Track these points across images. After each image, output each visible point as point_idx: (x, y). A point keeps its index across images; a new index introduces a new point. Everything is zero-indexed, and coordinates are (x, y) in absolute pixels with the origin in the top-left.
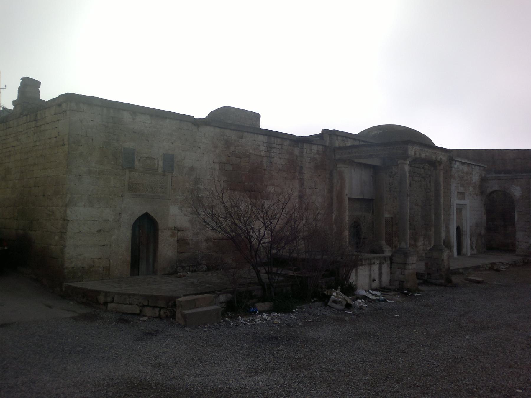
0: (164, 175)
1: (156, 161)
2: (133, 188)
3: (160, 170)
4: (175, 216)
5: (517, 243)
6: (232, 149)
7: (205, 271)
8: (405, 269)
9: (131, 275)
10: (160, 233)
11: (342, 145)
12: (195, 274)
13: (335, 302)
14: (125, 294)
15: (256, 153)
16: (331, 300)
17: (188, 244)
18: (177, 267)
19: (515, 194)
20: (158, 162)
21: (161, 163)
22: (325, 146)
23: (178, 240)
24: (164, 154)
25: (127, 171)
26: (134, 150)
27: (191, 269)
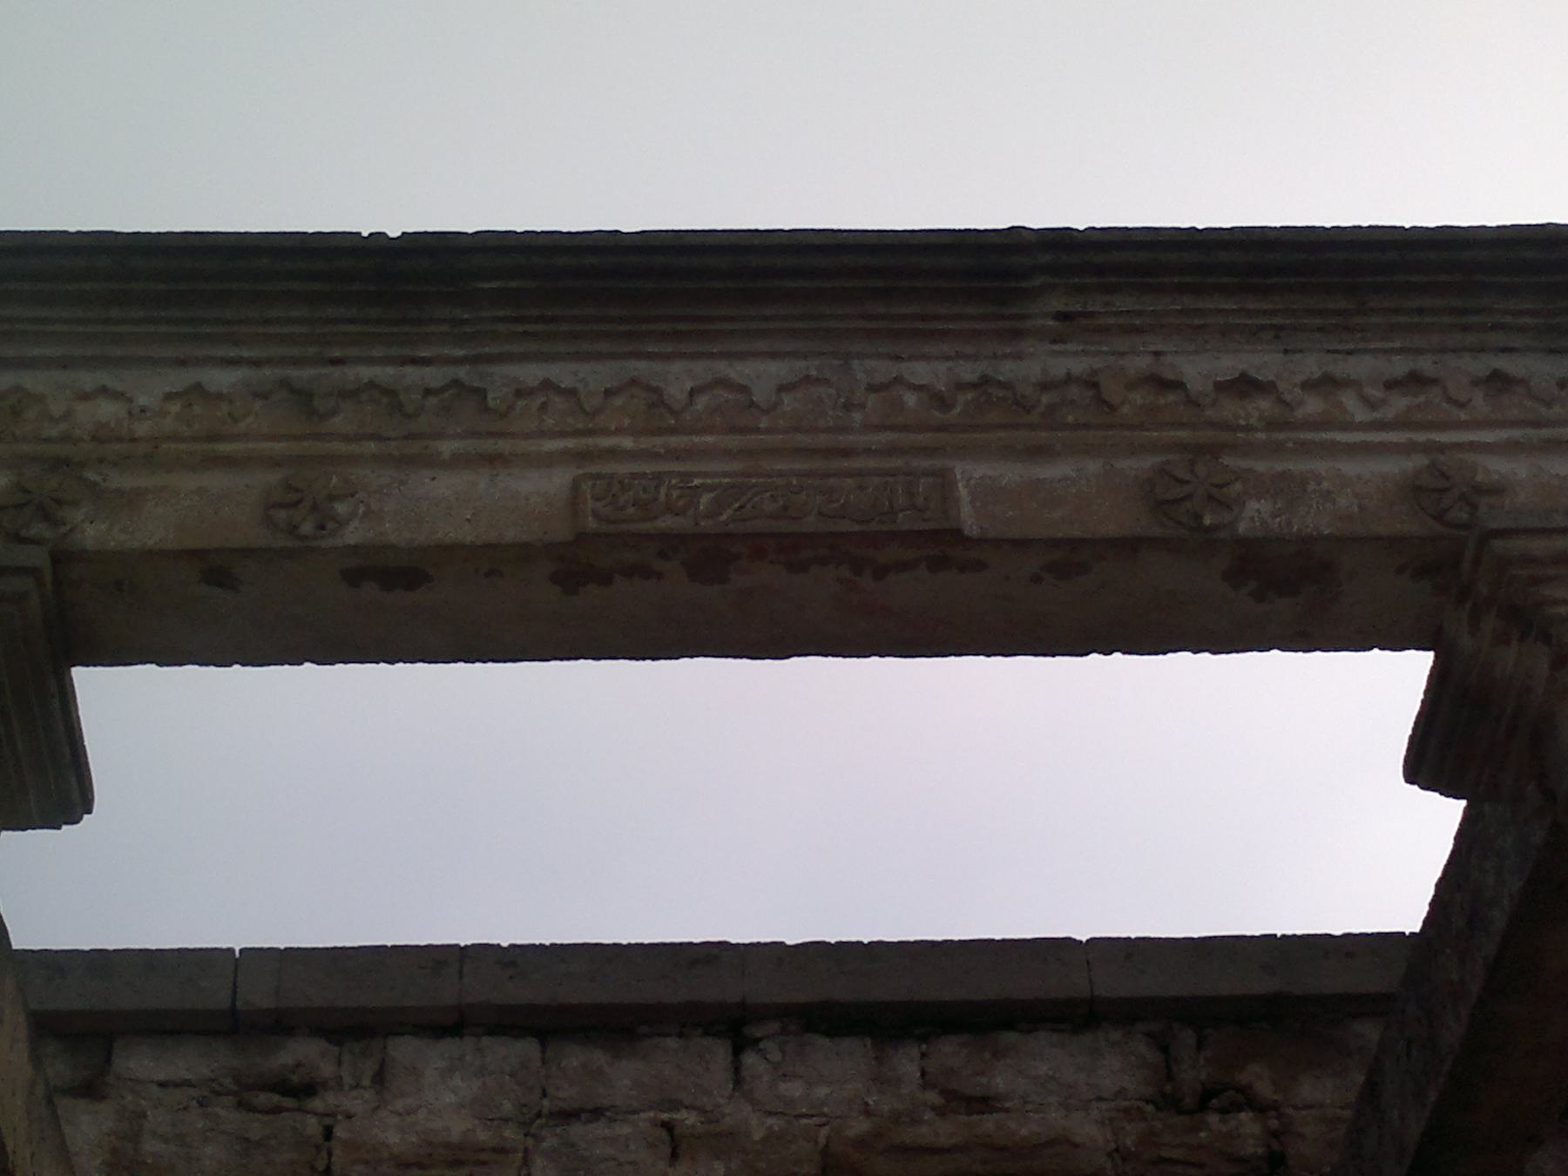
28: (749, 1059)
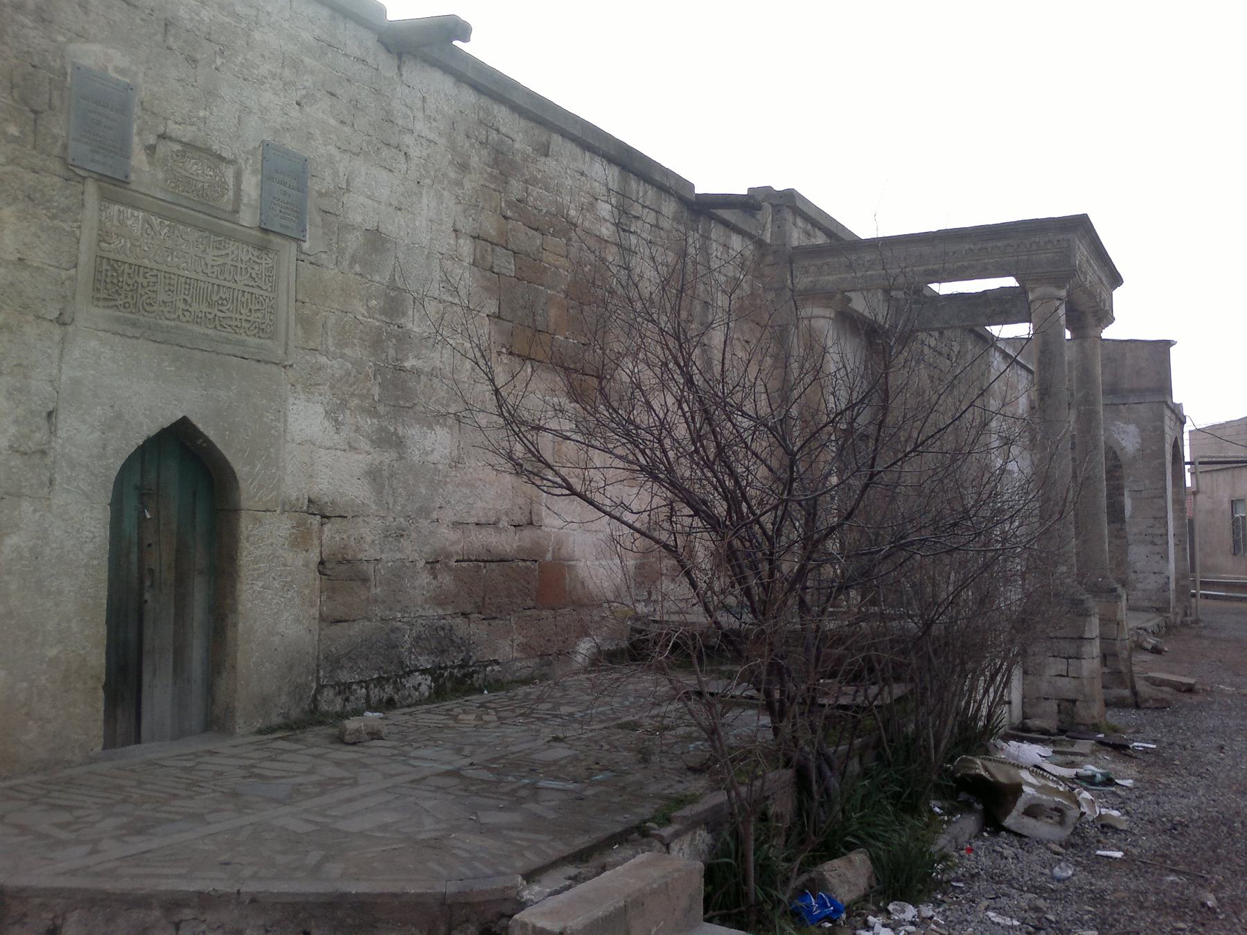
0: (263, 248)
1: (230, 173)
2: (120, 288)
3: (248, 218)
4: (305, 448)
5: (1133, 576)
6: (516, 188)
7: (430, 700)
8: (1078, 657)
9: (110, 742)
10: (245, 525)
11: (805, 242)
12: (397, 715)
13: (1033, 811)
14: (141, 902)
15: (587, 224)
16: (1021, 805)
17: (365, 580)
18: (320, 688)
19: (1124, 443)
20: (238, 176)
21: (251, 186)
22: (760, 243)
23: (322, 563)
24: (265, 145)
25: (91, 188)
26: (129, 88)
27: (375, 693)
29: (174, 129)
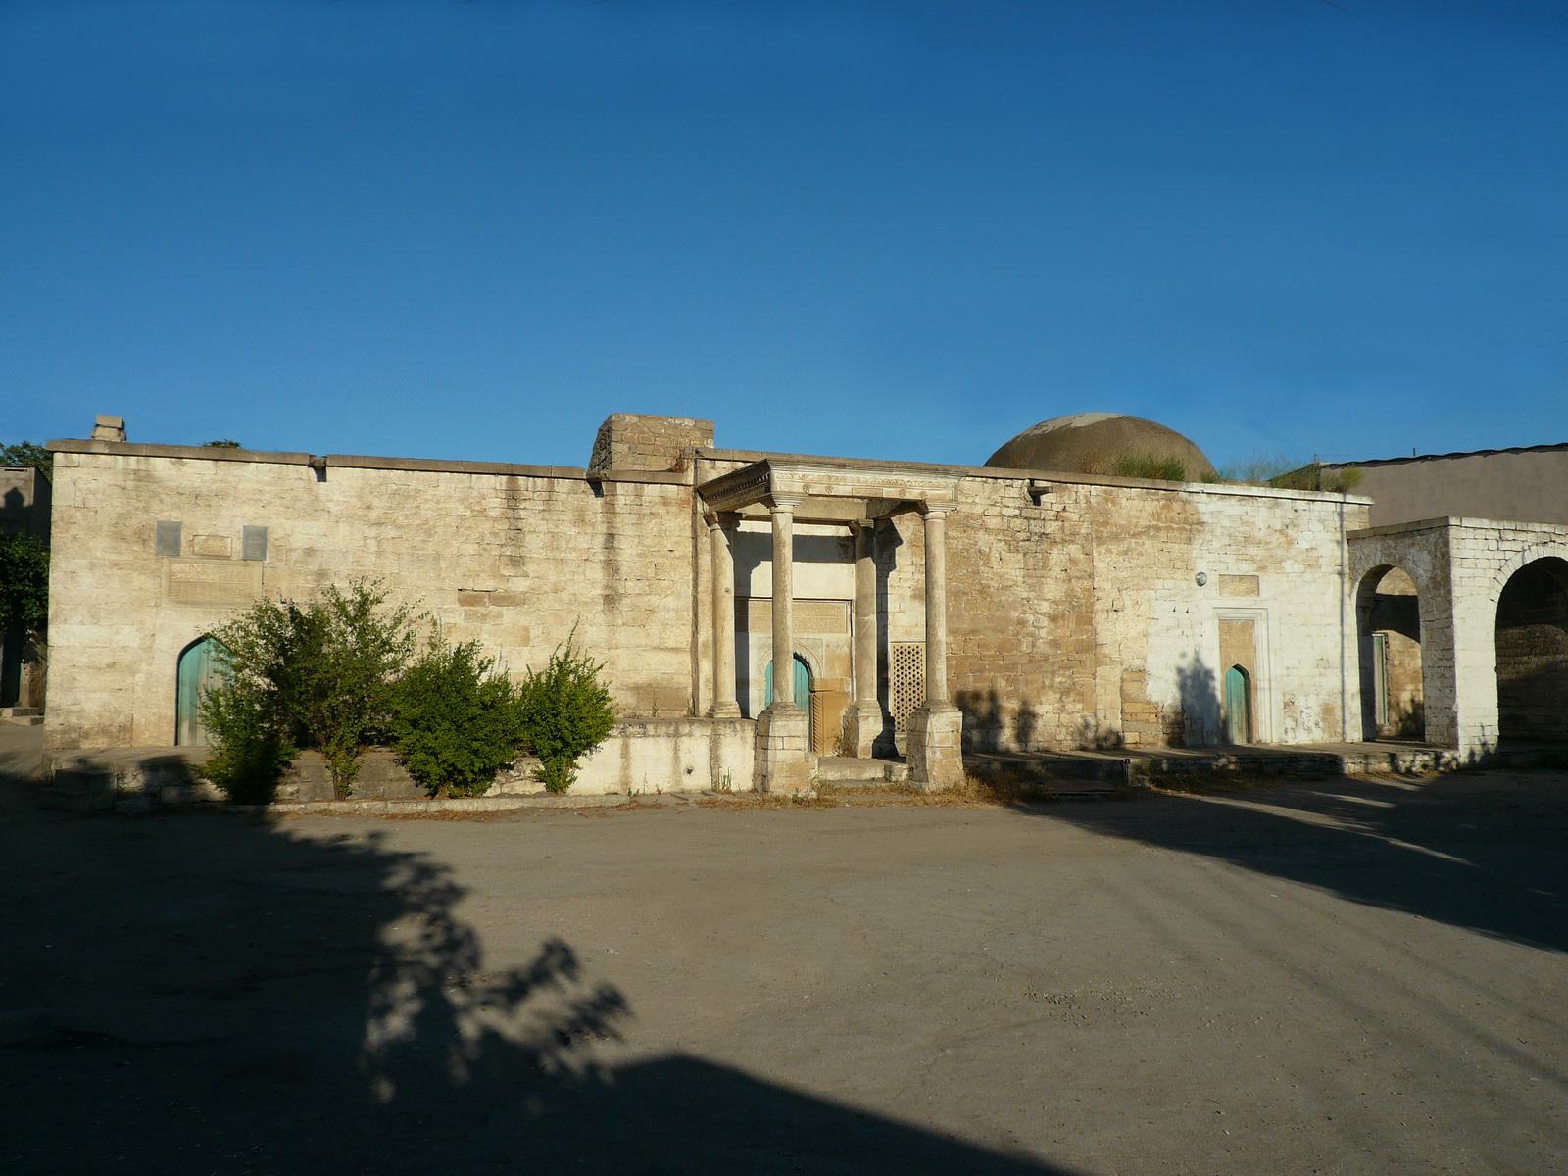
28: (1003, 543)
29: (200, 532)
